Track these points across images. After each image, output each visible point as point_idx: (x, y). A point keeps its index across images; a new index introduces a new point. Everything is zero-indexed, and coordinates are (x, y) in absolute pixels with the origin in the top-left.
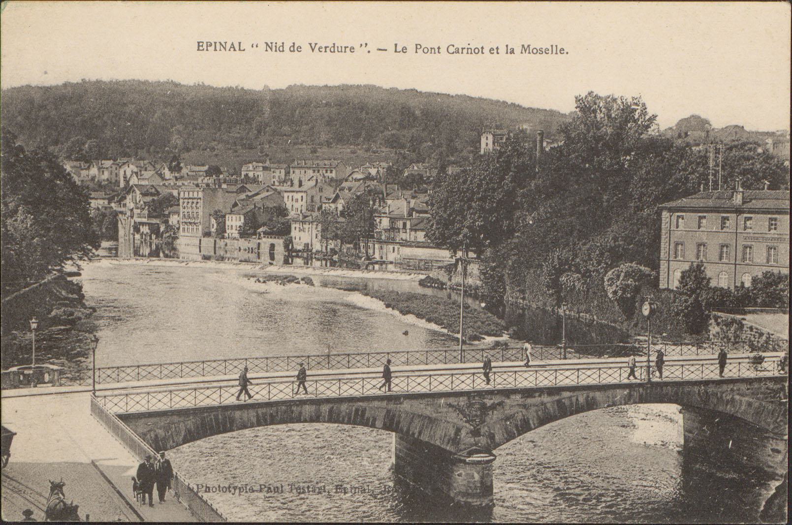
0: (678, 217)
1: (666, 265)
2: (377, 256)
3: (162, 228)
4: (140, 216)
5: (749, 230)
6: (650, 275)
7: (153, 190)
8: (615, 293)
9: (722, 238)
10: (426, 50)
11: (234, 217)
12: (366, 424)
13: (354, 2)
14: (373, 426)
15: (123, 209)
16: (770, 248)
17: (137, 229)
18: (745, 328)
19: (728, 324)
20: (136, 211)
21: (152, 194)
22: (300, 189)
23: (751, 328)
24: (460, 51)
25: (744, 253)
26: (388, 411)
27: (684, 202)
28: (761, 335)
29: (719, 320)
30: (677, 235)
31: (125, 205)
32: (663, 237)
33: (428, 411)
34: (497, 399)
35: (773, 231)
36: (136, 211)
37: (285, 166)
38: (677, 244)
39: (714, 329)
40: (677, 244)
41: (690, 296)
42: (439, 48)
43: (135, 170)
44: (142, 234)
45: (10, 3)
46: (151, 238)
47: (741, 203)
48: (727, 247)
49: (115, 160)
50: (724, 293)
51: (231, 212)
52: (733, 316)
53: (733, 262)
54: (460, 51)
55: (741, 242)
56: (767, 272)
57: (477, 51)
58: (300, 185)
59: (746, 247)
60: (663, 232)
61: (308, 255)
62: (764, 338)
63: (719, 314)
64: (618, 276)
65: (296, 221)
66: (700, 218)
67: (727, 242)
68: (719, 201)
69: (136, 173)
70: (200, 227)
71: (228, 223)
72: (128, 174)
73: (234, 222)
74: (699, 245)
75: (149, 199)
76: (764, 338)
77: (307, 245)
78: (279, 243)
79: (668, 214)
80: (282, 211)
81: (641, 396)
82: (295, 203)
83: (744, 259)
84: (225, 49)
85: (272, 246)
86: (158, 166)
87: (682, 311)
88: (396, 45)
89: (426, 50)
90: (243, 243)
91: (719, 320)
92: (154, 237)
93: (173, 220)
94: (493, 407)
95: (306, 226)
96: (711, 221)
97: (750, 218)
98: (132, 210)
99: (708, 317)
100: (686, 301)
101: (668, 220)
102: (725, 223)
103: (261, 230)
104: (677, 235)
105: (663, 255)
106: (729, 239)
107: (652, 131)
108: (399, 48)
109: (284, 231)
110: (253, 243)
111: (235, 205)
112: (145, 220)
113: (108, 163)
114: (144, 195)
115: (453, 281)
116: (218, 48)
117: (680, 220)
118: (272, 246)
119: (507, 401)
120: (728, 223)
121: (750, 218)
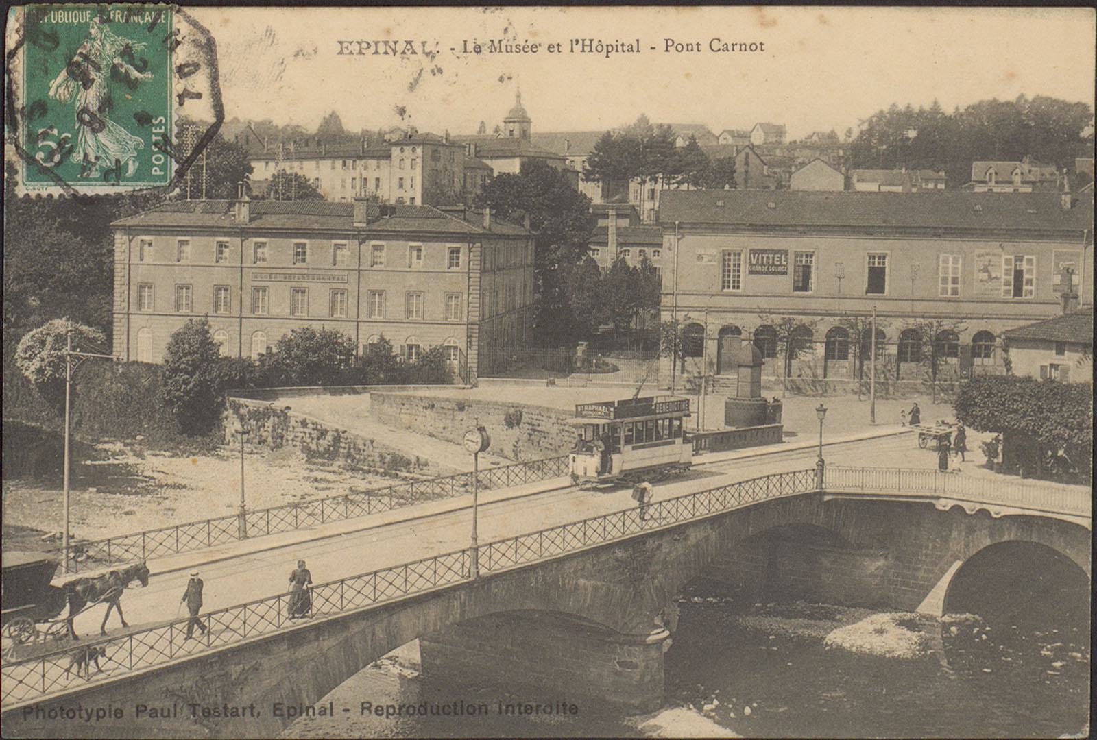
0: (375, 248)
1: (124, 321)
5: (260, 264)
6: (95, 339)
8: (40, 371)
9: (220, 276)
10: (680, 48)
16: (296, 290)
18: (293, 423)
19: (259, 416)
23: (304, 424)
24: (730, 48)
26: (59, 564)
27: (153, 218)
28: (323, 433)
29: (242, 411)
35: (298, 265)
38: (142, 287)
39: (232, 424)
41: (192, 374)
47: (247, 219)
48: (226, 290)
50: (244, 365)
52: (267, 403)
53: (236, 313)
54: (730, 48)
55: (249, 283)
56: (305, 330)
57: (753, 47)
59: (257, 289)
62: (329, 437)
63: (242, 401)
64: (43, 343)
66: (221, 245)
67: (229, 282)
68: (207, 216)
74: (180, 287)
76: (329, 437)
79: (125, 238)
84: (395, 52)
87: (179, 398)
88: (465, 42)
89: (680, 48)
91: (242, 411)
96: (197, 249)
97: (263, 244)
99: (223, 404)
100: (186, 382)
101: (126, 246)
102: (221, 252)
104: (138, 276)
106: (230, 279)
107: (787, 140)
108: (470, 47)
117: (146, 247)
120: (226, 252)
121: (263, 244)
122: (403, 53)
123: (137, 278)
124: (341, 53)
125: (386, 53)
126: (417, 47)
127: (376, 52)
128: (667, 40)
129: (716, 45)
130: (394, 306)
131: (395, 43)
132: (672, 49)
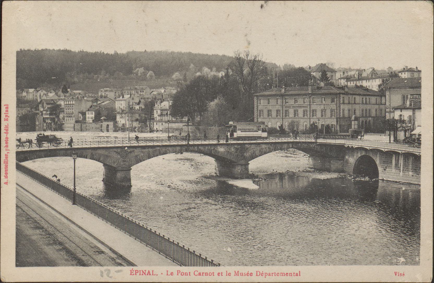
2: (155, 128)
3: (56, 119)
4: (46, 114)
7: (52, 102)
9: (278, 107)
11: (90, 112)
12: (84, 157)
13: (353, 1)
14: (86, 158)
15: (38, 112)
17: (44, 121)
20: (44, 112)
21: (52, 104)
22: (123, 99)
25: (286, 113)
30: (260, 107)
31: (38, 110)
32: (255, 108)
33: (106, 153)
34: (132, 150)
36: (44, 112)
37: (120, 89)
40: (260, 111)
42: (190, 273)
43: (46, 93)
44: (47, 123)
45: (432, 7)
46: (51, 125)
49: (36, 88)
51: (88, 110)
54: (271, 275)
55: (284, 109)
58: (123, 97)
60: (255, 106)
61: (123, 129)
65: (119, 113)
69: (45, 94)
70: (74, 118)
71: (87, 116)
72: (42, 94)
73: (90, 116)
75: (49, 106)
77: (123, 124)
78: (111, 124)
80: (113, 110)
81: (186, 149)
82: (120, 105)
83: (286, 116)
85: (108, 125)
86: (57, 91)
88: (167, 271)
89: (182, 274)
90: (94, 125)
92: (53, 124)
93: (61, 116)
94: (131, 152)
95: (123, 115)
96: (273, 101)
98: (42, 112)
103: (102, 118)
105: (255, 116)
109: (114, 119)
110: (98, 126)
111: (91, 107)
112: (48, 116)
113: (31, 90)
114: (47, 104)
115: (182, 135)
116: (141, 274)
118: (108, 125)
119: (136, 150)
122: (147, 275)
123: (259, 109)
124: (131, 274)
125: (142, 275)
126: (151, 273)
127: (140, 275)
128: (136, 271)
129: (196, 273)
130: (319, 114)
131: (145, 271)
132: (180, 274)
